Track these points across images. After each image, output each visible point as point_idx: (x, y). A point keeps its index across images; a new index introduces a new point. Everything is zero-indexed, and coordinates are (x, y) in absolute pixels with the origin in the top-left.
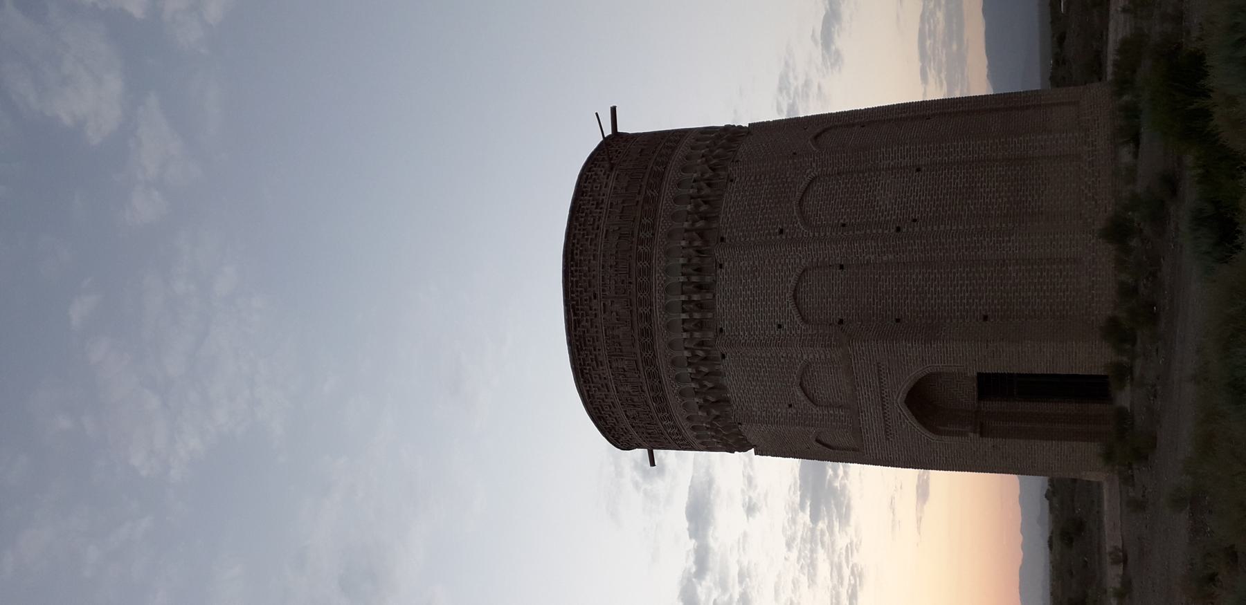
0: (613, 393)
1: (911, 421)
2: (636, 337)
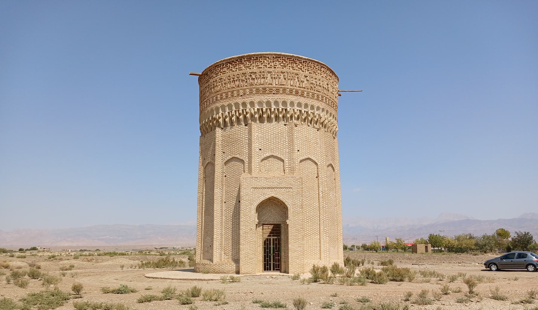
0: (268, 69)
1: (263, 198)
2: (295, 88)
